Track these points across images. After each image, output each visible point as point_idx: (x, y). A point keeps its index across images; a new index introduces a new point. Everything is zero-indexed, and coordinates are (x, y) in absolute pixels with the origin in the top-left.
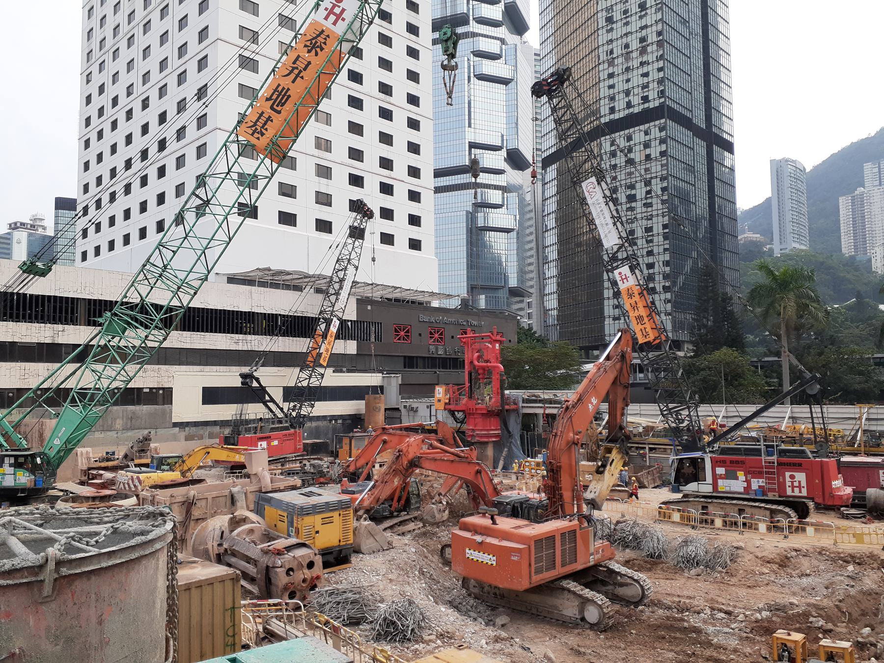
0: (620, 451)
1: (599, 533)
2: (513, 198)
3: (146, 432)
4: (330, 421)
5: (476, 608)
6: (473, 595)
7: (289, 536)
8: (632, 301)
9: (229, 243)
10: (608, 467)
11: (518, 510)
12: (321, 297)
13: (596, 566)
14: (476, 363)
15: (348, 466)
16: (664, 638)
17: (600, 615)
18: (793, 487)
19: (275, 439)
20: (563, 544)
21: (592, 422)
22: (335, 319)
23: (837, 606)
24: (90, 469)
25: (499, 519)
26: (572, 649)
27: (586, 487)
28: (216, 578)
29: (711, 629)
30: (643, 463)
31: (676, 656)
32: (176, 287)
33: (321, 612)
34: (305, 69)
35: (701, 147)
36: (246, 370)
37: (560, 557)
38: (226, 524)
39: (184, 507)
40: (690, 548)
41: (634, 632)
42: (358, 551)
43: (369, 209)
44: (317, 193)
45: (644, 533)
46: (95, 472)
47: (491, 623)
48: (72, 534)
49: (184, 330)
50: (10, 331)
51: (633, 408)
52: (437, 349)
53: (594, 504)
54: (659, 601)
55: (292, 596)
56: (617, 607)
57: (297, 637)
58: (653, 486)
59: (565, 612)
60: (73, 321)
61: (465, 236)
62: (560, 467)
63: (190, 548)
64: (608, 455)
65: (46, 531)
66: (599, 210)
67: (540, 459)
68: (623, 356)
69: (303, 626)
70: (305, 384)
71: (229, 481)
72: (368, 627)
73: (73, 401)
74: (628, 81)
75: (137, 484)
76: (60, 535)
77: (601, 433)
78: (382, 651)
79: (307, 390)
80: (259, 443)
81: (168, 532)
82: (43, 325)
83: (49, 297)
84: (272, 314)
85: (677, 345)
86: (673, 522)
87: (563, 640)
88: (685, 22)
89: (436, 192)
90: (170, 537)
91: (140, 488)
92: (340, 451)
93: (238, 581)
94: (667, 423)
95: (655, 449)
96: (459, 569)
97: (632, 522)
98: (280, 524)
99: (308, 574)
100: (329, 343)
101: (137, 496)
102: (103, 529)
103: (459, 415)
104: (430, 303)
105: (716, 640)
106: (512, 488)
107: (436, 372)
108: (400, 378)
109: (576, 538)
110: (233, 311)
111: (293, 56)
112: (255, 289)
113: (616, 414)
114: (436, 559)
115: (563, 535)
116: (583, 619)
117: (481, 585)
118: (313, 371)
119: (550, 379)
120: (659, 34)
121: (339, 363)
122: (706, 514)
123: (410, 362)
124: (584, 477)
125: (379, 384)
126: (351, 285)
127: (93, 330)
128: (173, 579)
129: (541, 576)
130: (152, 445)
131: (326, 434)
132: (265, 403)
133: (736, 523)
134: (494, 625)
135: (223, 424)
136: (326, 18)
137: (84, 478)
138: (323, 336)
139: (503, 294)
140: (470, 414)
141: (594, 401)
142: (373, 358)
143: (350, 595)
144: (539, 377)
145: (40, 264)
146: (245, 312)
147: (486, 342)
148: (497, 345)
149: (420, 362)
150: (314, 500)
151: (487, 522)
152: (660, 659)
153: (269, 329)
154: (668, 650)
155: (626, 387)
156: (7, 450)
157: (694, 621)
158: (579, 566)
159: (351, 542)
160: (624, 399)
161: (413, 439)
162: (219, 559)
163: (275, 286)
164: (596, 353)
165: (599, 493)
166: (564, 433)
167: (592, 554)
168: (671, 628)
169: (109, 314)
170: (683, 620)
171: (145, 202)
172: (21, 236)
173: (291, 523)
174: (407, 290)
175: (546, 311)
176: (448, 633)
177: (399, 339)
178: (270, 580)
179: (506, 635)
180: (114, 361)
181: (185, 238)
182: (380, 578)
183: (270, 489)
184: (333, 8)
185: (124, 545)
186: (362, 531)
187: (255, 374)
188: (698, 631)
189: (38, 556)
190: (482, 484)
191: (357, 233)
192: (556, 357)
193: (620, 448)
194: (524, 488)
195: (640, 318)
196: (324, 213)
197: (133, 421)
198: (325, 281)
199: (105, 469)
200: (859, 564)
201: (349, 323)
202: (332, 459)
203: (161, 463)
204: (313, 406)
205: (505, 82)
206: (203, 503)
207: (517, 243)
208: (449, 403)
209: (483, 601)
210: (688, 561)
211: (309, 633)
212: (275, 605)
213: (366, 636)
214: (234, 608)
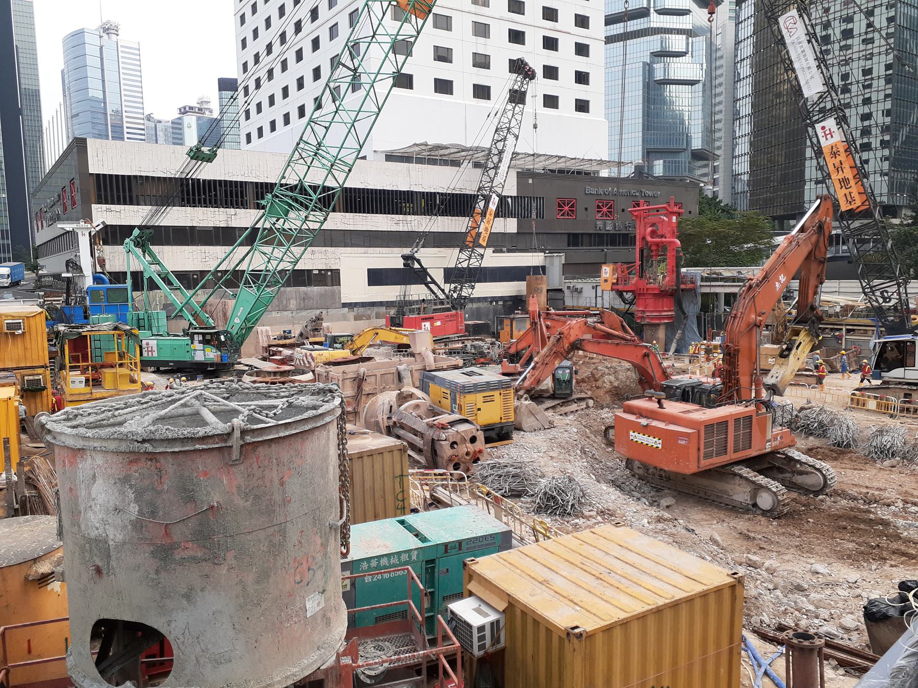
0: (809, 333)
1: (780, 420)
2: (700, 43)
3: (318, 312)
4: (491, 302)
5: (640, 488)
6: (637, 476)
7: (453, 412)
8: (836, 161)
9: (378, 114)
10: (794, 351)
11: (688, 394)
12: (479, 171)
13: (773, 453)
14: (649, 239)
15: (509, 348)
16: (845, 528)
17: (774, 502)
19: (439, 320)
20: (737, 429)
21: (779, 301)
22: (494, 196)
24: (270, 346)
25: (666, 403)
26: (741, 533)
27: (766, 372)
28: (385, 448)
29: (901, 522)
30: (837, 346)
31: (857, 547)
32: (329, 165)
33: (483, 484)
36: (407, 251)
37: (733, 443)
38: (394, 399)
39: (356, 383)
40: (886, 438)
42: (519, 429)
43: (530, 68)
44: (475, 54)
45: (832, 421)
46: (274, 349)
47: (656, 504)
48: (253, 407)
49: (347, 212)
50: (189, 215)
51: (828, 285)
52: (605, 225)
53: (774, 390)
54: (843, 491)
55: (456, 467)
56: (794, 495)
57: (460, 504)
59: (735, 497)
60: (243, 205)
61: (641, 92)
62: (738, 351)
63: (362, 420)
64: (794, 338)
65: (231, 404)
66: (800, 51)
68: (821, 228)
69: (467, 495)
70: (465, 265)
71: (396, 359)
72: (529, 500)
73: (247, 282)
75: (311, 360)
76: (244, 408)
77: (790, 313)
78: (541, 522)
79: (467, 271)
80: (423, 324)
81: (336, 407)
82: (217, 209)
83: (220, 181)
84: (431, 193)
85: (890, 210)
86: (868, 410)
87: (731, 525)
90: (339, 412)
91: (313, 364)
92: (501, 332)
93: (405, 451)
94: (869, 302)
95: (853, 330)
96: (623, 451)
97: (818, 409)
99: (471, 447)
100: (488, 222)
101: (313, 371)
103: (628, 296)
104: (598, 172)
105: (905, 534)
106: (684, 372)
107: (603, 250)
108: (563, 258)
109: (751, 424)
110: (392, 191)
112: (413, 166)
113: (808, 293)
114: (599, 439)
115: (737, 420)
116: (755, 505)
117: (646, 467)
118: (472, 252)
119: (735, 255)
121: (499, 242)
122: (909, 402)
123: (574, 240)
124: (767, 360)
126: (510, 157)
128: (344, 449)
129: (710, 461)
130: (325, 325)
131: (488, 315)
132: (427, 285)
134: (658, 505)
136: (827, 139)
137: (266, 355)
138: (482, 214)
139: (684, 158)
140: (640, 294)
141: (782, 278)
142: (535, 237)
143: (511, 469)
144: (722, 252)
145: (205, 149)
146: (404, 191)
147: (662, 215)
148: (674, 218)
149: (586, 239)
150: (475, 379)
151: (653, 406)
152: (838, 549)
153: (428, 209)
154: (848, 541)
155: (822, 262)
156: (195, 328)
157: (882, 513)
158: (753, 453)
159: (513, 420)
160: (818, 276)
161: (574, 322)
162: (389, 431)
163: (432, 162)
164: (792, 222)
166: (745, 314)
167: (769, 441)
168: (854, 519)
169: (269, 196)
171: (302, 78)
172: (191, 121)
173: (454, 401)
174: (573, 159)
175: (735, 177)
176: (609, 510)
177: (563, 215)
178: (435, 451)
179: (670, 516)
180: (280, 244)
181: (336, 112)
182: (541, 454)
185: (298, 418)
186: (522, 410)
187: (416, 255)
188: (886, 523)
189: (225, 425)
190: (649, 367)
191: (517, 97)
192: (743, 228)
193: (809, 330)
194: (698, 372)
195: (844, 182)
196: (482, 77)
197: (306, 301)
198: (483, 153)
199: (283, 346)
201: (509, 200)
202: (494, 340)
203: (333, 341)
206: (372, 379)
207: (703, 97)
208: (617, 283)
209: (648, 482)
211: (473, 502)
212: (440, 475)
213: (527, 508)
214: (402, 475)
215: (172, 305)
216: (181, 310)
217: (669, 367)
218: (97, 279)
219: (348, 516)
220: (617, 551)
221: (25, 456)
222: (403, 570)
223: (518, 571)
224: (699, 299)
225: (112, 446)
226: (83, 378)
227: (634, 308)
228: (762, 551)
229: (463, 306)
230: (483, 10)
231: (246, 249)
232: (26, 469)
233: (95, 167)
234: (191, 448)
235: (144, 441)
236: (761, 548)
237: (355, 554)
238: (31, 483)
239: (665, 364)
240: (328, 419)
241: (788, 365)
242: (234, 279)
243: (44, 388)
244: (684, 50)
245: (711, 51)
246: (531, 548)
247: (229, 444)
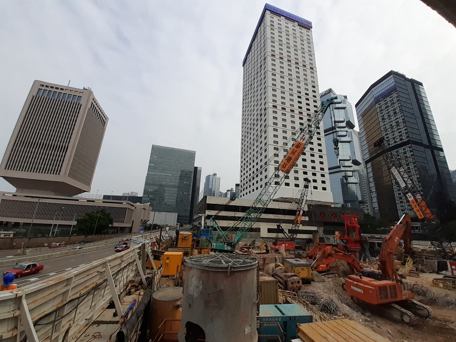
1: (406, 288)
2: (356, 173)
3: (254, 239)
7: (292, 272)
9: (275, 194)
10: (407, 263)
11: (371, 275)
12: (297, 204)
14: (349, 224)
17: (410, 319)
22: (301, 210)
24: (242, 247)
27: (398, 270)
34: (295, 152)
35: (429, 152)
36: (278, 224)
41: (425, 328)
42: (313, 281)
45: (427, 290)
46: (243, 248)
47: (364, 314)
51: (414, 242)
52: (335, 220)
53: (402, 276)
54: (436, 317)
55: (293, 291)
58: (429, 272)
63: (265, 272)
67: (377, 258)
69: (297, 301)
70: (294, 228)
72: (318, 306)
74: (393, 135)
78: (322, 315)
88: (413, 114)
89: (329, 174)
90: (257, 265)
92: (306, 249)
93: (277, 283)
97: (421, 285)
98: (289, 268)
99: (298, 285)
100: (300, 217)
102: (241, 260)
103: (345, 241)
106: (368, 267)
114: (340, 288)
116: (403, 320)
117: (357, 299)
120: (403, 120)
121: (304, 223)
128: (259, 277)
134: (365, 315)
135: (273, 238)
136: (301, 140)
137: (241, 250)
150: (298, 262)
151: (359, 278)
157: (451, 326)
158: (398, 299)
162: (273, 276)
164: (396, 222)
165: (404, 272)
169: (248, 210)
170: (446, 325)
172: (229, 193)
176: (347, 314)
182: (321, 290)
183: (285, 258)
185: (246, 265)
187: (281, 225)
191: (306, 187)
196: (297, 182)
204: (297, 235)
205: (349, 142)
210: (448, 303)
211: (299, 304)
215: (220, 235)
216: (222, 236)
217: (362, 265)
218: (204, 227)
219: (259, 300)
220: (351, 330)
221: (182, 270)
222: (276, 323)
223: (315, 331)
224: (369, 244)
225: (199, 267)
226: (197, 251)
227: (347, 245)
228: (408, 339)
229: (294, 240)
231: (240, 222)
232: (181, 274)
234: (218, 270)
235: (206, 267)
236: (407, 338)
237: (261, 315)
238: (181, 278)
239: (360, 264)
240: (254, 267)
241: (405, 268)
242: (236, 229)
243: (189, 253)
244: (352, 175)
245: (360, 175)
246: (319, 323)
247: (227, 271)
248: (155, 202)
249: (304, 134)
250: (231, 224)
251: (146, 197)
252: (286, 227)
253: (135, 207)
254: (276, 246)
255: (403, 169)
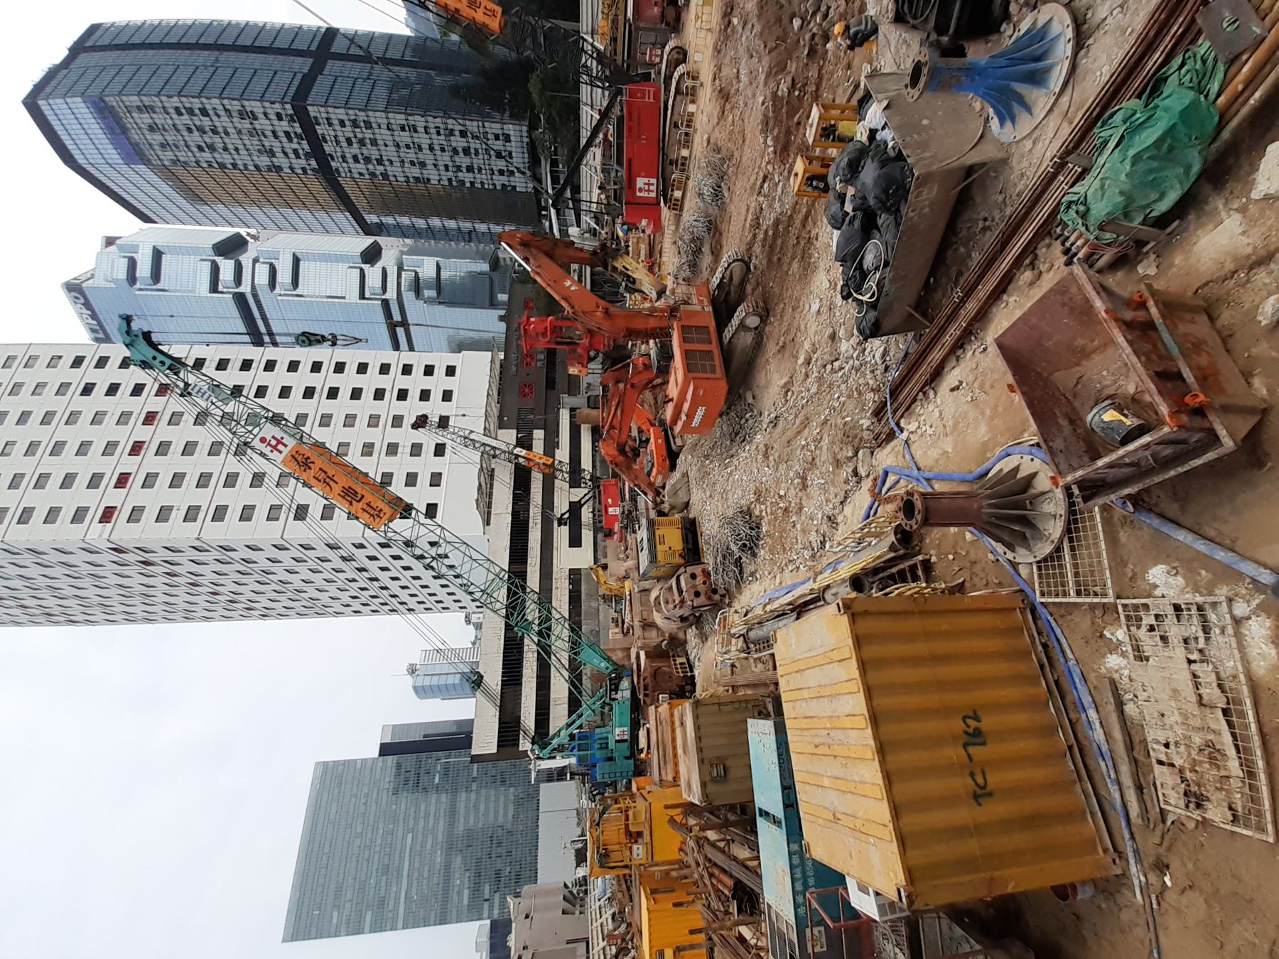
0: (614, 258)
10: (629, 273)
18: (649, 191)
23: (770, 52)
34: (325, 473)
111: (313, 482)
116: (756, 328)
121: (551, 445)
123: (551, 384)
125: (568, 412)
127: (526, 641)
133: (687, 134)
136: (280, 452)
139: (496, 276)
148: (533, 319)
157: (768, 220)
158: (712, 324)
168: (772, 247)
169: (516, 629)
180: (549, 628)
184: (271, 446)
188: (777, 222)
200: (732, 9)
204: (584, 470)
206: (644, 613)
230: (377, 447)
233: (493, 749)
242: (575, 669)
248: (508, 869)
249: (258, 439)
250: (560, 688)
251: (491, 908)
252: (564, 497)
253: (522, 952)
254: (616, 530)
255: (398, 56)
